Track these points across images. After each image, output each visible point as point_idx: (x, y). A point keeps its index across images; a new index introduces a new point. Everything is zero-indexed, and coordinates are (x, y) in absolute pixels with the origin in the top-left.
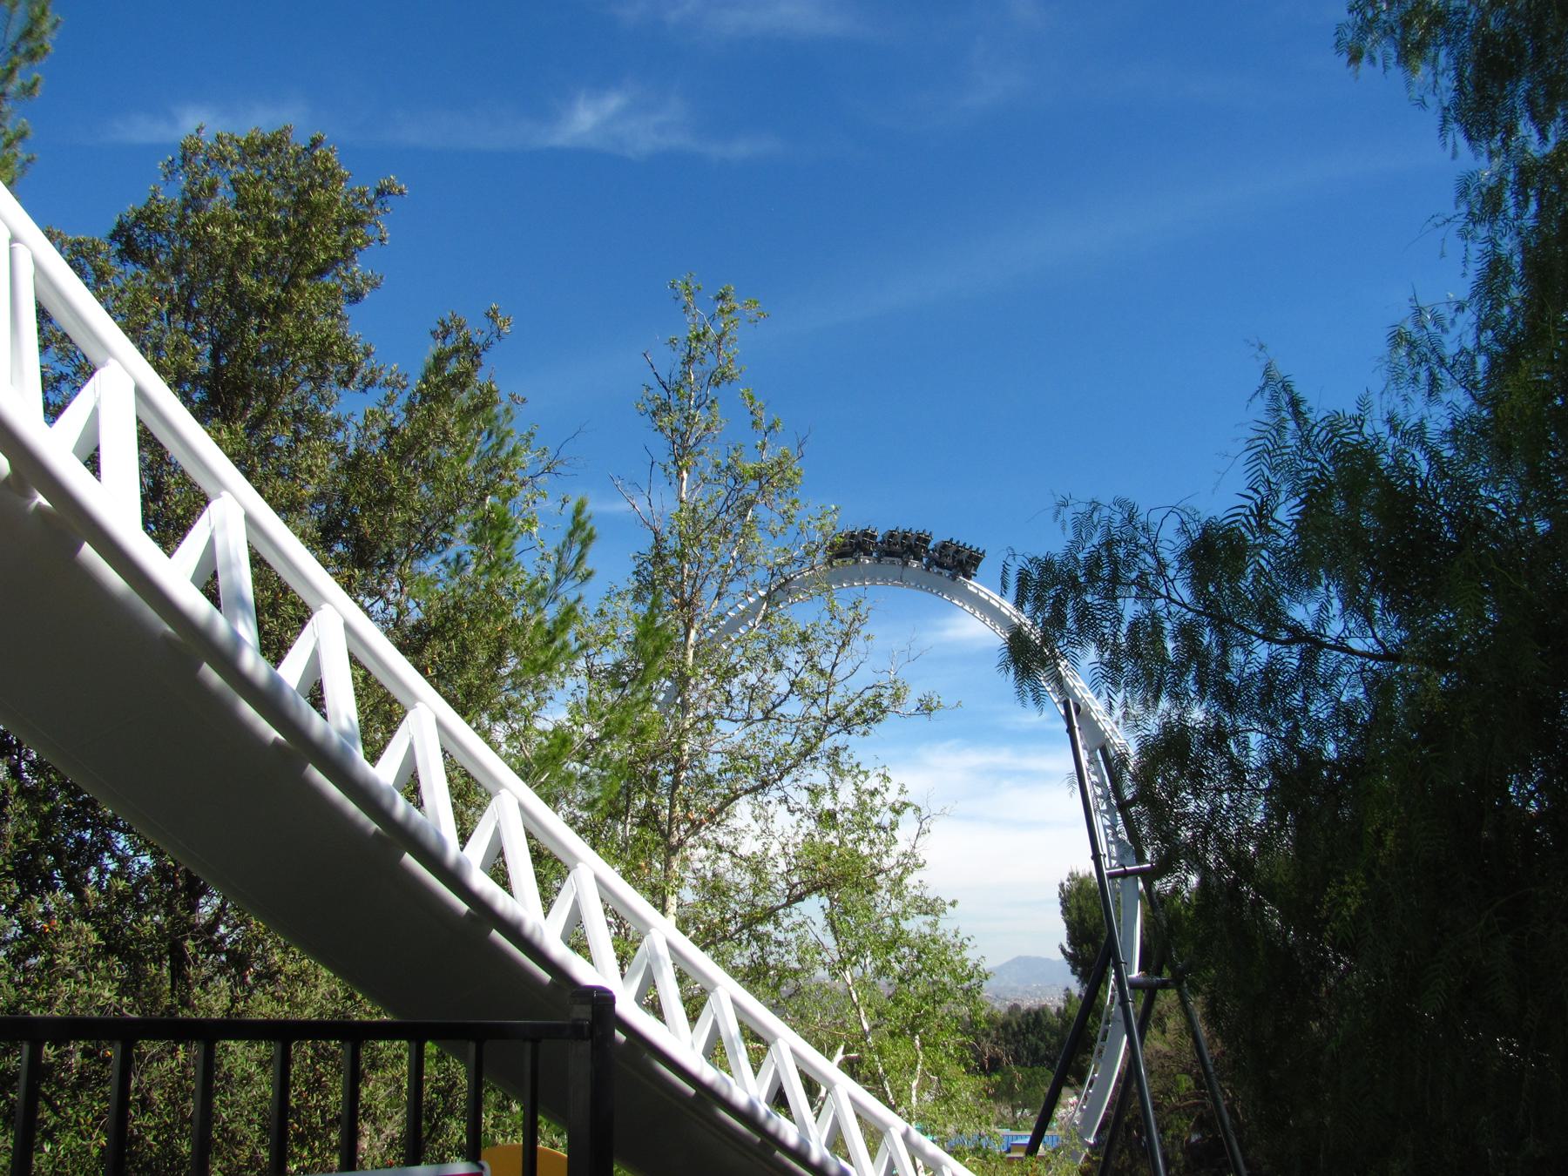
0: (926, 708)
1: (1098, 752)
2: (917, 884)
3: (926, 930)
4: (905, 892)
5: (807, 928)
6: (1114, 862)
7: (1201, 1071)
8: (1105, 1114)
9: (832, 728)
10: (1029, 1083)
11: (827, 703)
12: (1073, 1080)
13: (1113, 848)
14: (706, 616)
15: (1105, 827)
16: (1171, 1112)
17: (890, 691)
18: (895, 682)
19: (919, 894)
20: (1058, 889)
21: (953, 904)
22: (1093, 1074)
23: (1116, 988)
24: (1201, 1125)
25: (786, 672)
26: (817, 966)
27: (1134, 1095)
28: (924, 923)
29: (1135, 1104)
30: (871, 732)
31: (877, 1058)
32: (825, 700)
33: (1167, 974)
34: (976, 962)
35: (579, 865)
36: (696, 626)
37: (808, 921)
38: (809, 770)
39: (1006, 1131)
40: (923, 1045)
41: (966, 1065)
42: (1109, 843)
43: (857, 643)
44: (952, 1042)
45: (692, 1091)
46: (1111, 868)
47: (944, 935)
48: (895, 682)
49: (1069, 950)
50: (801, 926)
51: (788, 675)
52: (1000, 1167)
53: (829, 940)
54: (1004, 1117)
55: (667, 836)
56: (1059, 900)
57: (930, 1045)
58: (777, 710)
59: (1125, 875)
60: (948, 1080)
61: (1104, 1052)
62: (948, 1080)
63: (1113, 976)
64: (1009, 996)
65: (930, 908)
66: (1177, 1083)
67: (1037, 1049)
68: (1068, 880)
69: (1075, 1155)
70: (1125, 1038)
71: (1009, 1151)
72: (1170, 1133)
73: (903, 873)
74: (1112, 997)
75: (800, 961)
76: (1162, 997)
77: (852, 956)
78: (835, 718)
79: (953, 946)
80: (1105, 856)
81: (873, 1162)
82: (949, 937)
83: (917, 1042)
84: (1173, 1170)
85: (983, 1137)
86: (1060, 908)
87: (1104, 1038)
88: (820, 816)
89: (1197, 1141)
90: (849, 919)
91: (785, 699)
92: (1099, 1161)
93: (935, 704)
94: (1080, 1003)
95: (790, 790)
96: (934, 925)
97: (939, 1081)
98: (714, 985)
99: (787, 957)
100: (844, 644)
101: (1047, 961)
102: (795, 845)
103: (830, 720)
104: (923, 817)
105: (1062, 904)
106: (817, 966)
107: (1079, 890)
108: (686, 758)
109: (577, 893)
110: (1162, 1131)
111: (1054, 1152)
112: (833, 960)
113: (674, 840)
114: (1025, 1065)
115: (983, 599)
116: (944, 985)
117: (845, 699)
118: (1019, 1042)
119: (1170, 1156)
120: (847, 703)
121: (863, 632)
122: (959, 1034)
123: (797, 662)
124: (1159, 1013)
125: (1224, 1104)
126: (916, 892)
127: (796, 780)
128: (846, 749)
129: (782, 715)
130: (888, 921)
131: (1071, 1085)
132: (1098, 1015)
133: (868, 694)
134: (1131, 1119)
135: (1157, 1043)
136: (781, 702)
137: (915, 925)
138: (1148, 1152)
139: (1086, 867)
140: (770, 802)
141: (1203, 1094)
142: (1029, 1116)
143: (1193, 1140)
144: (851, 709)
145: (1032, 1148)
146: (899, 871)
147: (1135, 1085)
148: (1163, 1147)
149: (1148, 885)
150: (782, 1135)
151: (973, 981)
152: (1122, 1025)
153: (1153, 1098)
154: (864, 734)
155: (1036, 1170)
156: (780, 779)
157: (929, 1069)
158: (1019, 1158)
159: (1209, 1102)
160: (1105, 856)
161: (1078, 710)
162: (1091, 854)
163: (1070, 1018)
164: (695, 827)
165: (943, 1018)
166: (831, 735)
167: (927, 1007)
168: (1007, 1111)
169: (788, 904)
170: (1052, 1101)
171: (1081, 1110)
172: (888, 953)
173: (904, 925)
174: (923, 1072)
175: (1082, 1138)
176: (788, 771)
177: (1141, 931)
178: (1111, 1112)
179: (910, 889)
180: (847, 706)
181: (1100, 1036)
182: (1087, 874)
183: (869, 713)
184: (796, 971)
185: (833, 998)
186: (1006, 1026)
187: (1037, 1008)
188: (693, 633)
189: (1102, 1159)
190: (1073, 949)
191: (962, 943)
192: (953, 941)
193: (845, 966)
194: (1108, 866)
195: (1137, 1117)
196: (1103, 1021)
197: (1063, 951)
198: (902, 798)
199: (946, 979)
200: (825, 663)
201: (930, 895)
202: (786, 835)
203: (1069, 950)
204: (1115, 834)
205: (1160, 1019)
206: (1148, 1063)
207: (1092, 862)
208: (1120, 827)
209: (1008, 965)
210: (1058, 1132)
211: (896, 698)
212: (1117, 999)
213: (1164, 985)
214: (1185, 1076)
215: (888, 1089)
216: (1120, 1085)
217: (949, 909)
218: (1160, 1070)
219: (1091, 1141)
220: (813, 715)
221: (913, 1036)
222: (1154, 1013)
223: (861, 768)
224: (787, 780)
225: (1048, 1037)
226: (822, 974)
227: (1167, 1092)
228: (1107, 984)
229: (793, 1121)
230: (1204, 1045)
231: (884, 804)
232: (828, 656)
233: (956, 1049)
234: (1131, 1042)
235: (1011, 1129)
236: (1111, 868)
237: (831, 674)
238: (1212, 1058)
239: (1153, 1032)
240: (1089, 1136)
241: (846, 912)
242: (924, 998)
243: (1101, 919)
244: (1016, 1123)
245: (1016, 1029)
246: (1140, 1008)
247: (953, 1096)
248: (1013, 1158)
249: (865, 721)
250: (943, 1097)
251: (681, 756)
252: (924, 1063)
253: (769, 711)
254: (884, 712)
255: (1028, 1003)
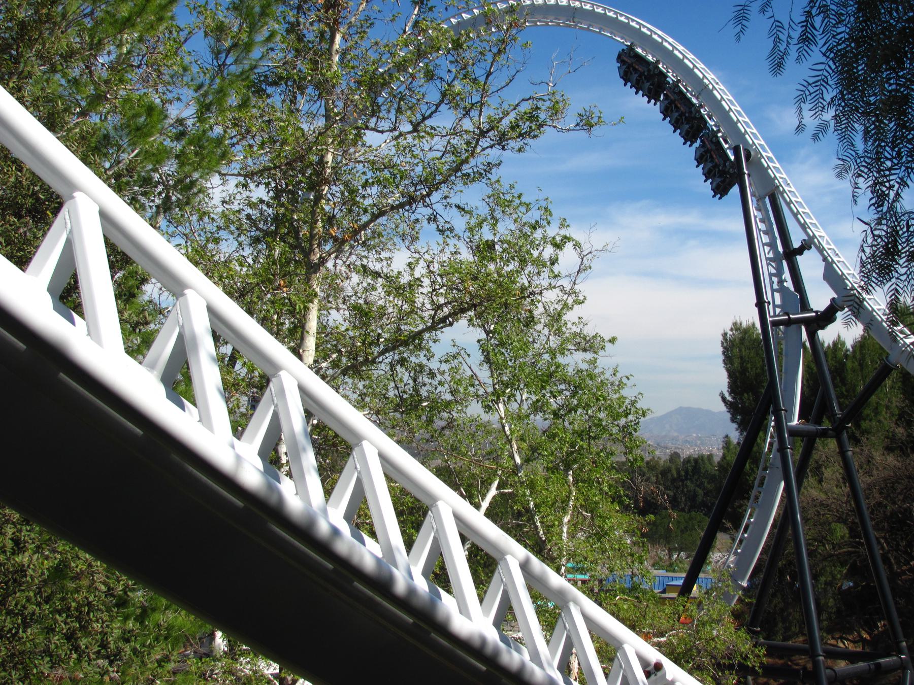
0: (587, 123)
1: (767, 200)
2: (577, 320)
3: (584, 366)
4: (564, 329)
5: (461, 359)
6: (778, 310)
7: (857, 521)
8: (759, 559)
9: (484, 143)
10: (686, 528)
11: (480, 115)
12: (729, 525)
13: (777, 296)
14: (353, 19)
15: (771, 275)
16: (825, 559)
17: (548, 104)
18: (553, 94)
19: (578, 331)
20: (721, 338)
21: (613, 340)
22: (749, 519)
23: (775, 435)
24: (853, 572)
25: (438, 82)
26: (470, 398)
27: (789, 540)
28: (583, 361)
29: (790, 549)
30: (527, 148)
31: (528, 493)
32: (477, 113)
33: (827, 424)
34: (633, 399)
35: (77, 194)
36: (341, 29)
37: (462, 352)
38: (459, 186)
39: (662, 572)
40: (576, 481)
41: (621, 503)
42: (773, 290)
43: (513, 53)
44: (607, 479)
45: (239, 503)
46: (775, 316)
47: (602, 373)
48: (553, 94)
49: (729, 398)
50: (454, 357)
51: (439, 85)
52: (652, 606)
53: (484, 374)
54: (661, 559)
55: (308, 253)
56: (721, 349)
57: (583, 481)
58: (428, 122)
59: (788, 323)
60: (601, 517)
61: (766, 482)
62: (601, 517)
63: (773, 423)
64: (670, 445)
65: (590, 344)
66: (831, 532)
67: (695, 495)
68: (732, 330)
69: (727, 597)
70: (783, 484)
71: (664, 591)
72: (823, 579)
73: (562, 309)
74: (771, 444)
75: (453, 392)
76: (821, 448)
77: (507, 388)
78: (488, 131)
79: (612, 384)
80: (769, 303)
81: (481, 601)
82: (608, 375)
83: (570, 478)
84: (824, 616)
85: (636, 575)
86: (722, 357)
87: (761, 484)
88: (478, 247)
89: (850, 588)
90: (503, 350)
91: (436, 111)
92: (751, 603)
93: (595, 120)
94: (738, 449)
95: (439, 208)
96: (593, 362)
97: (592, 518)
98: (276, 368)
99: (440, 388)
100: (499, 52)
101: (708, 413)
102: (441, 263)
103: (483, 134)
104: (585, 253)
105: (724, 353)
106: (470, 398)
107: (742, 340)
108: (329, 171)
109: (71, 231)
110: (815, 577)
111: (706, 593)
112: (486, 392)
113: (315, 258)
114: (683, 510)
115: (657, 41)
116: (600, 420)
117: (500, 111)
118: (678, 488)
119: (823, 602)
120: (501, 116)
121: (520, 39)
122: (614, 472)
123: (449, 71)
124: (817, 462)
125: (878, 552)
126: (575, 329)
127: (446, 197)
128: (499, 164)
129: (432, 128)
130: (546, 357)
131: (725, 530)
132: (756, 462)
133: (525, 107)
134: (785, 565)
135: (812, 491)
136: (432, 113)
137: (574, 361)
138: (800, 596)
139: (750, 316)
140: (417, 220)
141: (856, 542)
142: (684, 559)
143: (845, 587)
144: (505, 124)
145: (686, 589)
146: (559, 307)
147: (790, 532)
148: (814, 594)
149: (812, 336)
150: (355, 560)
151: (630, 417)
152: (779, 473)
153: (808, 544)
154: (520, 150)
155: (688, 610)
156: (429, 195)
157: (582, 506)
158: (673, 599)
159: (864, 551)
160: (769, 303)
161: (748, 156)
162: (755, 301)
163: (728, 464)
164: (339, 244)
165: (598, 454)
166: (483, 150)
167: (582, 443)
168: (664, 554)
169: (433, 328)
170: (706, 546)
171: (736, 553)
172: (543, 388)
173: (560, 359)
174: (575, 507)
175: (735, 580)
176: (437, 187)
177: (802, 382)
178: (764, 557)
179: (569, 325)
180: (501, 119)
181: (757, 482)
182: (751, 325)
183: (525, 126)
184: (448, 404)
185: (488, 433)
186: (665, 472)
187: (696, 456)
188: (338, 38)
189: (754, 601)
190: (733, 398)
191: (620, 381)
192: (611, 379)
193: (498, 398)
194: (772, 314)
195: (790, 563)
196: (761, 467)
197: (724, 399)
198: (563, 232)
199: (602, 415)
200: (479, 72)
201: (589, 331)
202: (431, 252)
203: (729, 398)
204: (781, 282)
205: (816, 468)
206: (804, 510)
207: (756, 309)
208: (787, 275)
209: (669, 415)
210: (712, 575)
211: (555, 111)
212: (776, 446)
213: (824, 434)
214: (839, 525)
215: (538, 524)
216: (776, 531)
217: (608, 346)
218: (816, 518)
219: (745, 584)
220: (465, 128)
221: (566, 471)
222: (812, 462)
223: (523, 199)
224: (436, 196)
225: (706, 484)
226: (475, 409)
227: (822, 540)
228: (766, 433)
229: (377, 541)
230: (861, 495)
231: (544, 237)
232: (483, 65)
233: (610, 486)
234: (788, 489)
235: (667, 571)
236: (775, 316)
237: (485, 83)
238: (868, 508)
239: (810, 480)
240: (743, 579)
241: (502, 344)
242: (580, 434)
243: (762, 368)
244: (671, 565)
245: (675, 475)
246: (798, 457)
247: (606, 533)
248: (665, 598)
249: (521, 135)
250: (595, 534)
251: (324, 168)
252: (577, 499)
253: (418, 124)
254: (541, 126)
255: (688, 451)
